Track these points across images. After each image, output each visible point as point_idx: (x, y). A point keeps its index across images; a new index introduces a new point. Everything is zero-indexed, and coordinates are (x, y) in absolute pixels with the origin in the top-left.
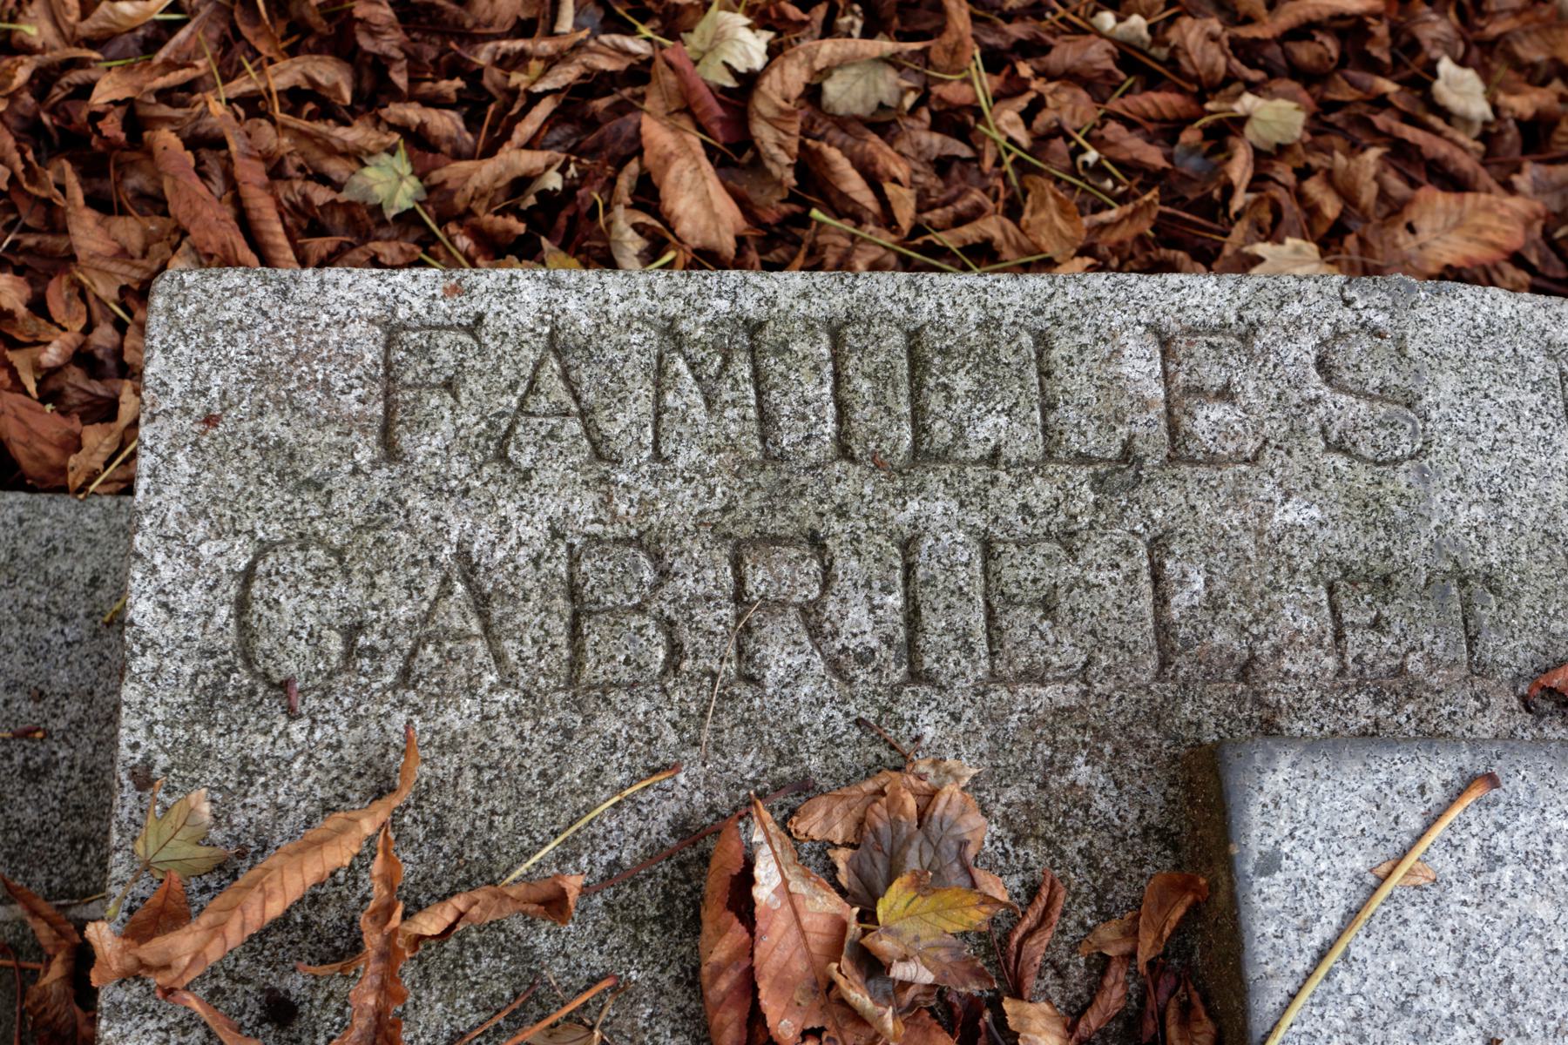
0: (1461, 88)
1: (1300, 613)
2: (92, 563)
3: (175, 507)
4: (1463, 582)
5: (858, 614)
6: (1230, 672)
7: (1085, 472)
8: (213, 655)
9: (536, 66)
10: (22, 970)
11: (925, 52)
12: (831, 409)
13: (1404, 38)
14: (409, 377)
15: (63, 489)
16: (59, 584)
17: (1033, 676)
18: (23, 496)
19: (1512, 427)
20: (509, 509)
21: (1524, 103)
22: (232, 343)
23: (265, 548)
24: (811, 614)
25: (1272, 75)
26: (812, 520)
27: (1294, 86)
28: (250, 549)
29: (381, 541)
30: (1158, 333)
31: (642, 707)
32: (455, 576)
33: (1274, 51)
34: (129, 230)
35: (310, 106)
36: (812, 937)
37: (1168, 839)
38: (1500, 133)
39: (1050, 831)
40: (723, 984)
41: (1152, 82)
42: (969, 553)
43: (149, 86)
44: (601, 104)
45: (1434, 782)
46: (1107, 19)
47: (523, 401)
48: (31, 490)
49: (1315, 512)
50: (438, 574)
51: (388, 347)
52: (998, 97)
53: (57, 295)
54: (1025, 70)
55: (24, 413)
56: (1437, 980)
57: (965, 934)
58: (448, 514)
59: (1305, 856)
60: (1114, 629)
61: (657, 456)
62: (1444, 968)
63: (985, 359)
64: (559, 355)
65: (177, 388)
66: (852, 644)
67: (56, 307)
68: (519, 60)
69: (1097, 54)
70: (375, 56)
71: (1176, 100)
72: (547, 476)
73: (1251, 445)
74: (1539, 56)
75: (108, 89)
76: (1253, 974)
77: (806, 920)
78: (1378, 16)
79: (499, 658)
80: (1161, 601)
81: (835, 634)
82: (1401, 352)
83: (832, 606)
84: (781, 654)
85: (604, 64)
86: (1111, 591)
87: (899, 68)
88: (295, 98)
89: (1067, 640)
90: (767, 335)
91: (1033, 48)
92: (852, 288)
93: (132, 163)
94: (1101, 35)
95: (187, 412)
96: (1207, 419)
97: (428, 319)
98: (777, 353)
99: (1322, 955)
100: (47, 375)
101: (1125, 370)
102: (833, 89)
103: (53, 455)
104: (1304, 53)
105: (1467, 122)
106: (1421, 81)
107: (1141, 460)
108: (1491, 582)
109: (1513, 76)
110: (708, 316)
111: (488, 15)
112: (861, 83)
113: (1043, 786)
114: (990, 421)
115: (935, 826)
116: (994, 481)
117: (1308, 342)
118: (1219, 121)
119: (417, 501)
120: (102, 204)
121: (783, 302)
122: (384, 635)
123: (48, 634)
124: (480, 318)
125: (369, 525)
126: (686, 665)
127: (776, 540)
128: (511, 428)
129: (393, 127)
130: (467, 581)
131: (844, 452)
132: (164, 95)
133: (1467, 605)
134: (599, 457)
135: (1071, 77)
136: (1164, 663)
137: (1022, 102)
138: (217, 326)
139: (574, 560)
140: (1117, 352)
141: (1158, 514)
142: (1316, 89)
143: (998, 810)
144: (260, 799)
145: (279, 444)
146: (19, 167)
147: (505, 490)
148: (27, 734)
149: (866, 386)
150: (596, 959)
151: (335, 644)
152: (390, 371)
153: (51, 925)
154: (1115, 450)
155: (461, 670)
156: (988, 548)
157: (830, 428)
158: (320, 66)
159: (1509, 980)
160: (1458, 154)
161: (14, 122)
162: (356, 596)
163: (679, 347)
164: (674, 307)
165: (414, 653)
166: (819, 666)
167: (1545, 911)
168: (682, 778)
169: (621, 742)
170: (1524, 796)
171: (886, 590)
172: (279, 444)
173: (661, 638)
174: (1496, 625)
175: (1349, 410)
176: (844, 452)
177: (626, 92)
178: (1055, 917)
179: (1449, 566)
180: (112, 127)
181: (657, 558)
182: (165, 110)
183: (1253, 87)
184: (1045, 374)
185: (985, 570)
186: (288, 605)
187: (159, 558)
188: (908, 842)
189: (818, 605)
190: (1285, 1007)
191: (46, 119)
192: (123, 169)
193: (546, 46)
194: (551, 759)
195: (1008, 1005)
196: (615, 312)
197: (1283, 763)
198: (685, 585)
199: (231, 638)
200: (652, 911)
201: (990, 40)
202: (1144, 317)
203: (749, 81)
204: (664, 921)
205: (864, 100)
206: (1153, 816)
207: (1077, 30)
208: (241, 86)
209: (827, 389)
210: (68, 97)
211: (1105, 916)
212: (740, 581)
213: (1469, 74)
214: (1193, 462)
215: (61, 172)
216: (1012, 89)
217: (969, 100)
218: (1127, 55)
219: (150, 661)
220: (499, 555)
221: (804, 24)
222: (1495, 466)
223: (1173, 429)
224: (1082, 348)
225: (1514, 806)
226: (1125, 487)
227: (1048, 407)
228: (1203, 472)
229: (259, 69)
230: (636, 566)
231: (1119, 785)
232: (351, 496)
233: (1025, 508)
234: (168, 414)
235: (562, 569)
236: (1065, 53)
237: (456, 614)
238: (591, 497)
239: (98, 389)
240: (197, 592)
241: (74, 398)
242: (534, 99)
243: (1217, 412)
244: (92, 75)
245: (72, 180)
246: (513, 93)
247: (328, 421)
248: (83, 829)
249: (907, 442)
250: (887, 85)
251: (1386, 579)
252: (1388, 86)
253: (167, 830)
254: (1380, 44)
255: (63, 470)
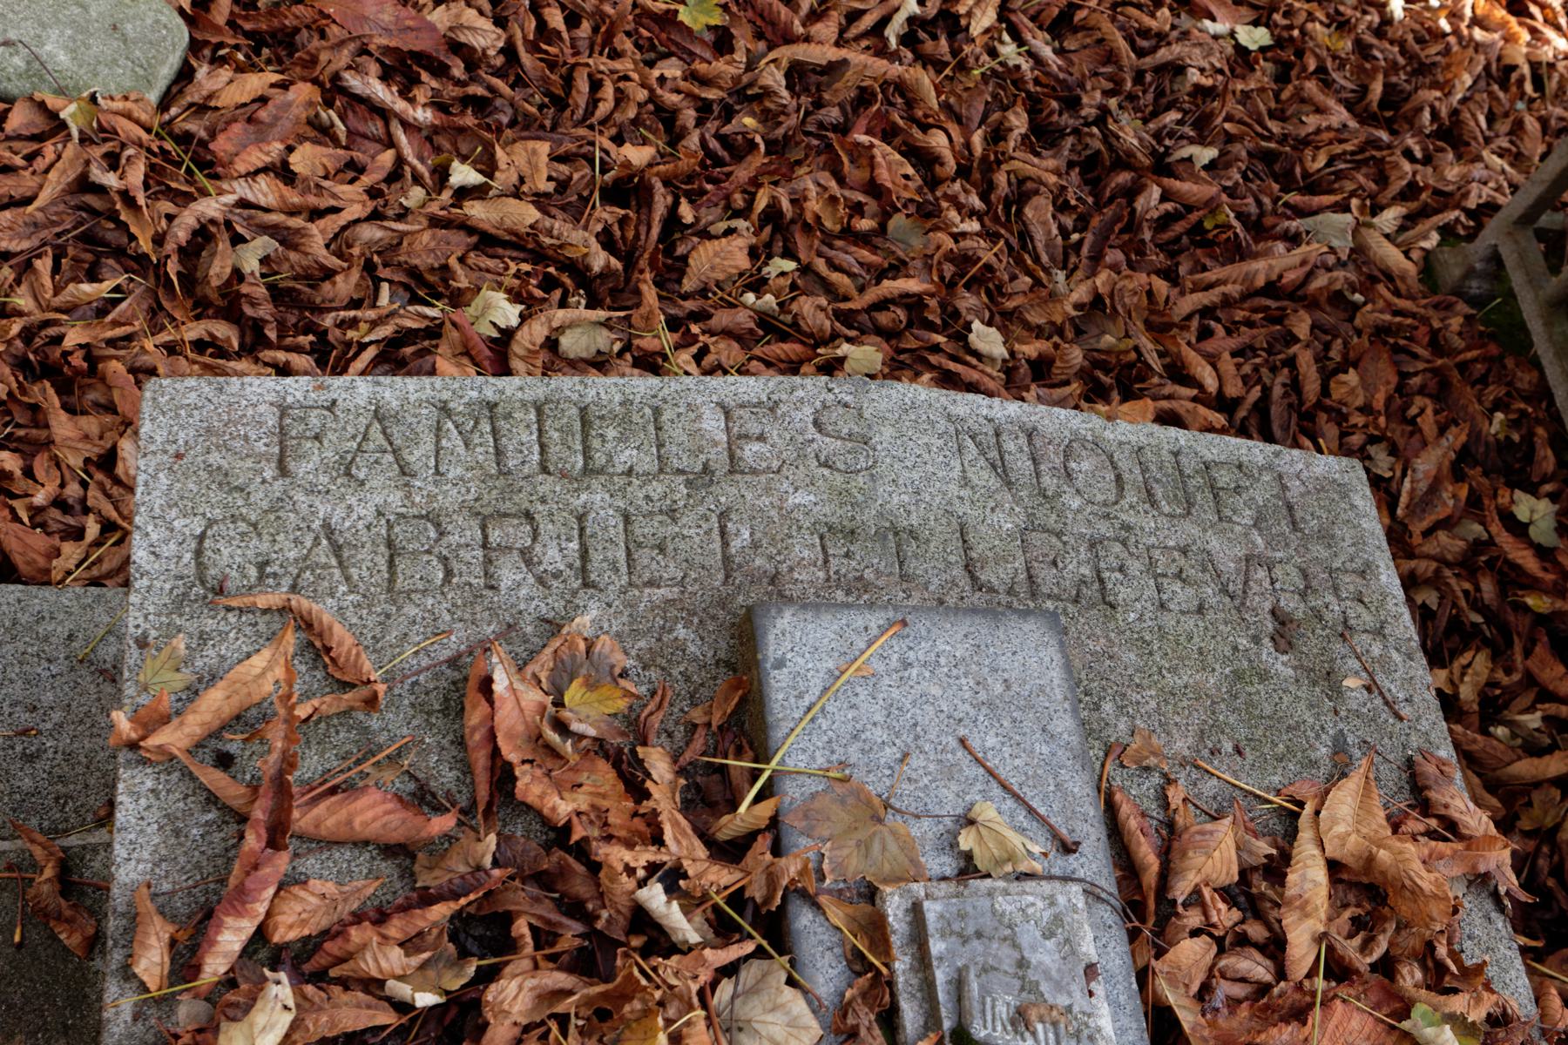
0: (987, 339)
1: (804, 549)
2: (69, 625)
3: (158, 501)
4: (896, 534)
5: (553, 553)
6: (765, 580)
7: (681, 478)
8: (182, 578)
9: (364, 326)
10: (23, 879)
11: (627, 318)
12: (536, 448)
13: (950, 309)
14: (294, 433)
15: (48, 583)
16: (46, 639)
17: (651, 583)
18: (20, 587)
19: (926, 456)
20: (353, 501)
21: (1031, 349)
22: (191, 416)
23: (211, 523)
24: (526, 554)
25: (863, 332)
26: (526, 505)
27: (879, 339)
28: (203, 523)
29: (279, 518)
30: (723, 407)
31: (430, 601)
32: (322, 536)
33: (864, 318)
34: (91, 424)
35: (210, 350)
36: (527, 713)
37: (729, 665)
38: (1016, 368)
39: (664, 663)
40: (477, 737)
41: (784, 337)
42: (616, 521)
43: (102, 336)
44: (409, 350)
45: (873, 625)
46: (750, 297)
47: (360, 445)
48: (25, 583)
49: (812, 497)
50: (312, 535)
51: (281, 418)
52: (678, 347)
53: (40, 464)
54: (695, 329)
55: (21, 534)
56: (875, 724)
57: (615, 715)
58: (317, 503)
59: (800, 660)
60: (698, 559)
61: (437, 472)
62: (879, 718)
63: (624, 421)
64: (380, 421)
65: (159, 439)
66: (550, 568)
67: (39, 473)
68: (353, 323)
69: (743, 319)
70: (254, 319)
71: (798, 347)
72: (374, 483)
73: (775, 464)
74: (1042, 321)
75: (74, 337)
76: (770, 719)
77: (523, 704)
78: (932, 295)
79: (348, 579)
80: (725, 544)
81: (540, 563)
82: (861, 416)
83: (538, 548)
84: (509, 573)
85: (409, 324)
86: (697, 539)
87: (611, 329)
88: (199, 345)
89: (672, 565)
90: (500, 410)
91: (701, 316)
92: (548, 385)
93: (89, 385)
94: (746, 307)
95: (165, 452)
96: (750, 451)
97: (305, 403)
98: (505, 418)
99: (809, 709)
100: (36, 511)
101: (704, 426)
102: (567, 342)
103: (41, 562)
104: (883, 318)
105: (993, 360)
106: (961, 336)
107: (713, 473)
108: (913, 534)
109: (1025, 333)
110: (466, 399)
111: (331, 295)
112: (585, 337)
113: (659, 640)
114: (627, 453)
115: (596, 657)
116: (630, 484)
117: (808, 410)
118: (827, 361)
119: (299, 496)
120: (70, 410)
121: (508, 393)
122: (281, 566)
123: (39, 670)
124: (334, 402)
125: (272, 510)
126: (455, 580)
127: (506, 515)
128: (353, 459)
129: (266, 364)
130: (329, 539)
131: (544, 469)
132: (111, 343)
133: (898, 545)
134: (404, 474)
135: (727, 333)
136: (727, 577)
137: (694, 349)
138: (182, 407)
139: (390, 526)
140: (699, 417)
141: (723, 499)
142: (894, 342)
143: (633, 653)
144: (211, 653)
145: (219, 468)
146: (14, 385)
147: (350, 491)
148: (25, 732)
149: (556, 435)
150: (405, 731)
151: (253, 572)
152: (283, 431)
153: (44, 848)
154: (699, 468)
155: (326, 584)
156: (627, 519)
157: (536, 457)
158: (218, 326)
159: (915, 725)
160: (986, 379)
161: (10, 360)
162: (265, 546)
163: (449, 417)
164: (446, 395)
165: (298, 576)
166: (531, 580)
167: (936, 691)
168: (453, 638)
169: (418, 620)
170: (924, 633)
171: (569, 540)
172: (219, 468)
173: (440, 566)
174: (916, 556)
175: (830, 445)
176: (544, 469)
177: (426, 343)
178: (666, 704)
179: (887, 525)
180: (77, 360)
181: (438, 525)
182: (112, 351)
183: (849, 340)
184: (658, 429)
185: (626, 530)
186: (226, 552)
187: (150, 528)
188: (581, 666)
189: (530, 549)
190: (788, 735)
191: (31, 357)
192: (84, 389)
193: (371, 314)
194: (378, 629)
195: (639, 749)
196: (412, 398)
197: (788, 614)
198: (454, 539)
199: (192, 570)
200: (437, 707)
201: (672, 312)
202: (715, 398)
203: (508, 334)
204: (445, 712)
205: (587, 349)
206: (722, 655)
207: (732, 306)
208: (164, 337)
209: (534, 437)
210: (45, 345)
211: (694, 705)
212: (485, 537)
213: (993, 330)
214: (742, 472)
215: (44, 390)
216: (687, 341)
217: (658, 349)
218: (764, 320)
219: (145, 582)
220: (347, 524)
221: (545, 300)
222: (915, 475)
223: (732, 457)
224: (679, 415)
225: (919, 639)
226: (704, 485)
227: (660, 446)
228: (748, 478)
229: (177, 327)
230: (426, 529)
231: (702, 639)
232: (261, 495)
233: (648, 498)
234: (154, 453)
235: (384, 532)
236: (722, 318)
237: (323, 554)
238: (400, 494)
239: (71, 521)
240: (172, 546)
241: (54, 527)
242: (363, 347)
243: (756, 447)
244: (63, 330)
245: (51, 392)
246: (348, 344)
247: (248, 456)
248: (64, 790)
249: (580, 463)
250: (604, 340)
251: (852, 532)
252: (940, 339)
253: (158, 663)
254: (933, 312)
255: (48, 571)
